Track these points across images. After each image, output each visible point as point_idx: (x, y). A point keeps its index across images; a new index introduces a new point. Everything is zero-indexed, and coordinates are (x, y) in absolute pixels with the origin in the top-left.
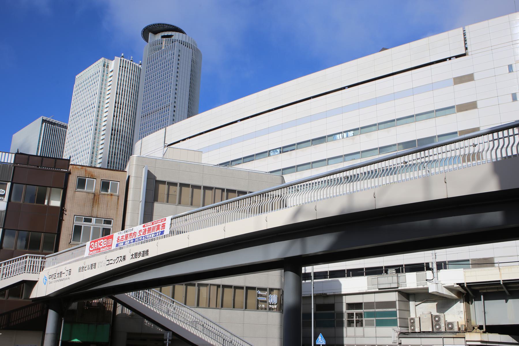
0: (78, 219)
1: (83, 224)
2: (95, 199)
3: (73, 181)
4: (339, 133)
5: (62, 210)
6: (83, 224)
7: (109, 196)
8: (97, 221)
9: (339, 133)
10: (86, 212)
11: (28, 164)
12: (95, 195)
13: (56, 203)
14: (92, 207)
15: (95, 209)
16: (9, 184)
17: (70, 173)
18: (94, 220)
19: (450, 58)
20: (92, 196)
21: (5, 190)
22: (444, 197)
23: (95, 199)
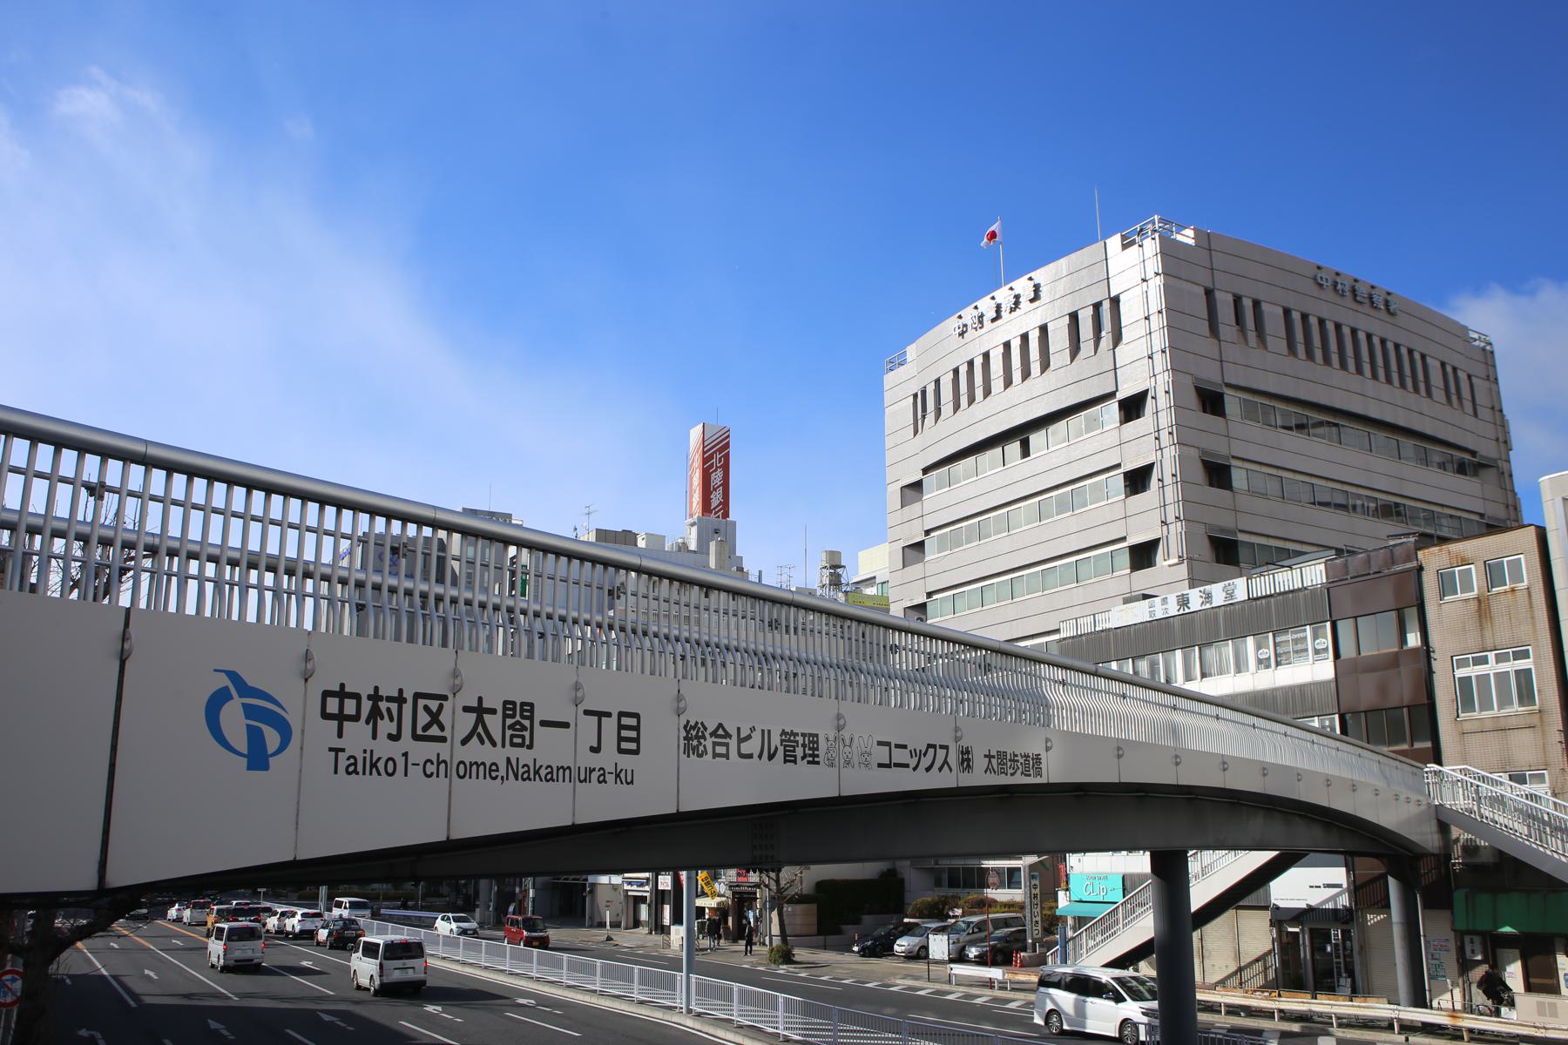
5: (1426, 649)
15: (1488, 634)
18: (1491, 656)
20: (1473, 606)
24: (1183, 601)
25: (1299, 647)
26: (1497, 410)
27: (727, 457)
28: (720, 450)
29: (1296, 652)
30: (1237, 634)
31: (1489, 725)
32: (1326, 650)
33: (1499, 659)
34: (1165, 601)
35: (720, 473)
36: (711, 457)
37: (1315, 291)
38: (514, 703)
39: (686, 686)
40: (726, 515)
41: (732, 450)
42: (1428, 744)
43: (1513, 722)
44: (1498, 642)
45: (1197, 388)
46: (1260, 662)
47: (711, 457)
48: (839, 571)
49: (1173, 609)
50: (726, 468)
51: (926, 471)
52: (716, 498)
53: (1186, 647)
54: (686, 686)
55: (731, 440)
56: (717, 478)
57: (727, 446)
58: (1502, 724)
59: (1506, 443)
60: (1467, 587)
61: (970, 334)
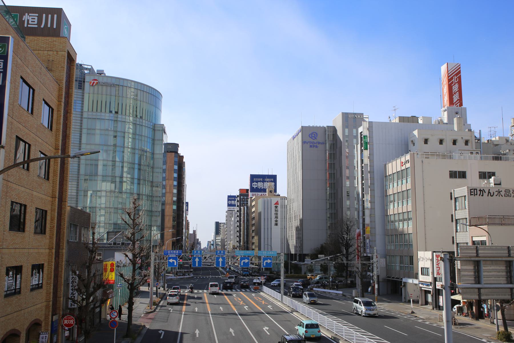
27: (460, 78)
28: (456, 75)
40: (461, 105)
41: (462, 74)
47: (452, 78)
52: (456, 98)
56: (455, 88)
57: (460, 72)
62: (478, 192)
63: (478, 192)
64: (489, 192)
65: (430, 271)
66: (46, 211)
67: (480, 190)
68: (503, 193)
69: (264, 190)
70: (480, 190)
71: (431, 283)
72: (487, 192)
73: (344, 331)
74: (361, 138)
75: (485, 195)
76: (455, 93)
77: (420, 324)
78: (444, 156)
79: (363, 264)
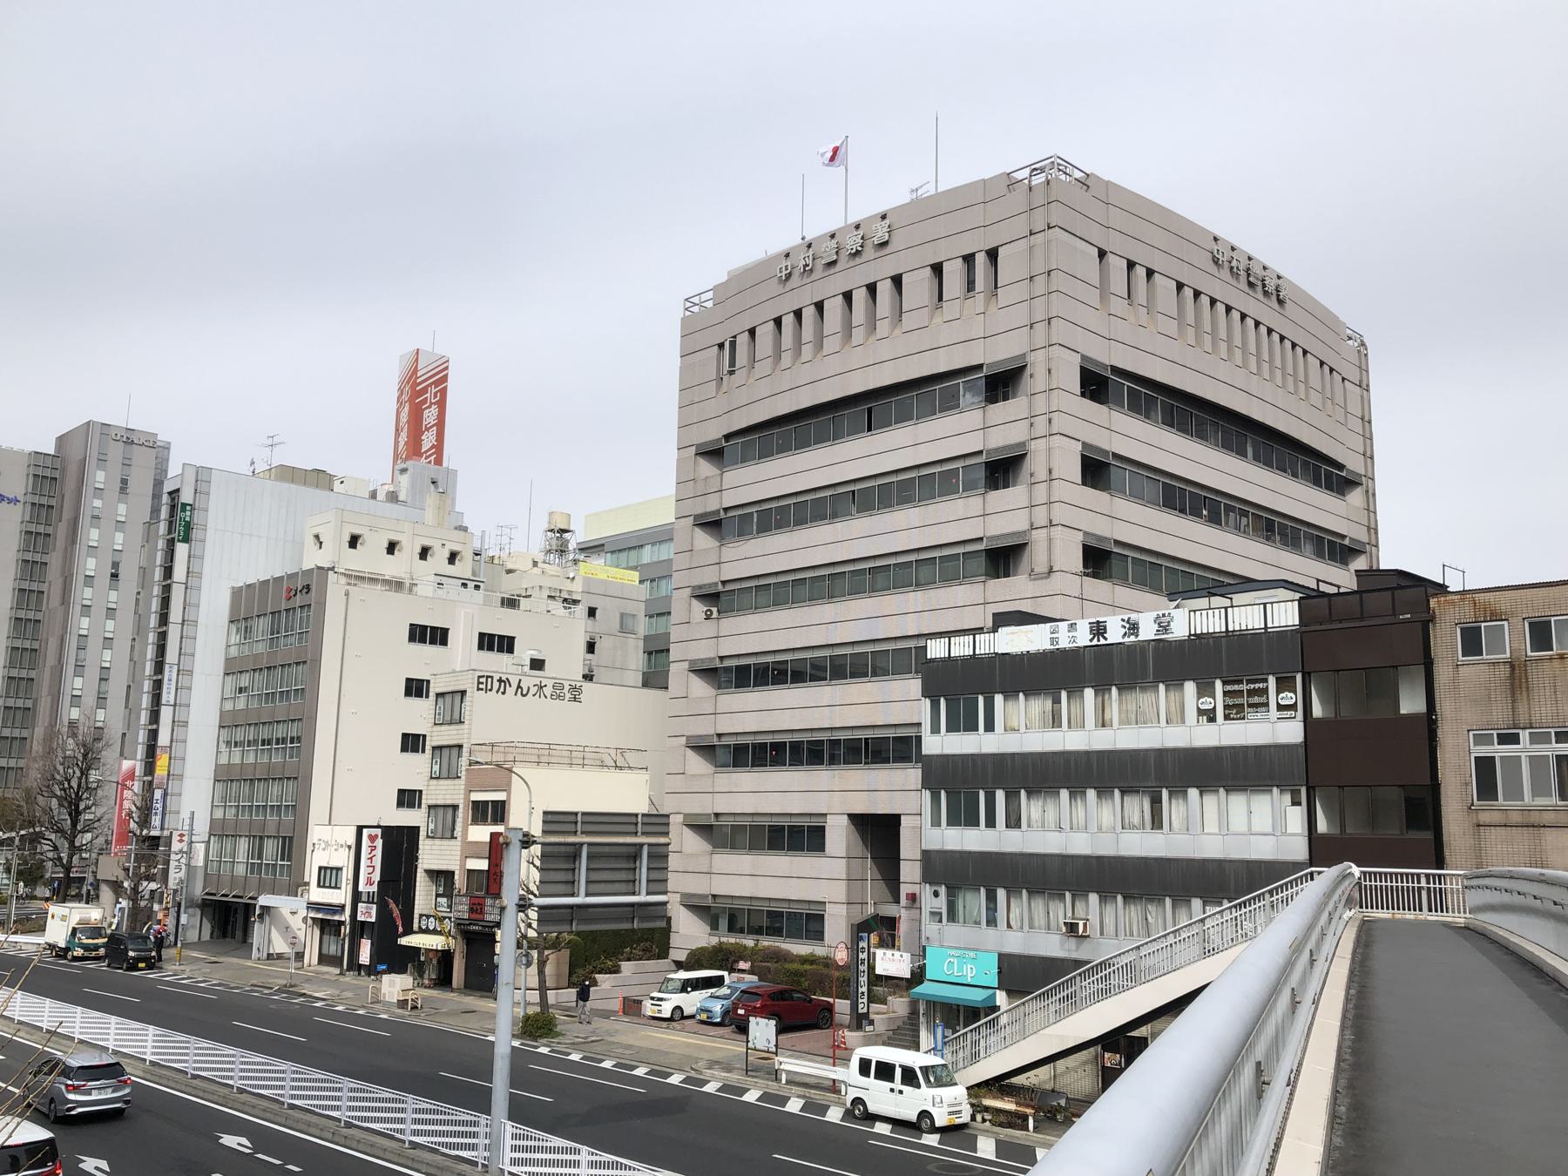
0: (1481, 740)
1: (1499, 751)
2: (1517, 676)
3: (1446, 640)
4: (940, 635)
5: (1429, 722)
6: (1499, 751)
7: (1556, 663)
8: (1534, 739)
9: (940, 635)
10: (1500, 715)
11: (1331, 621)
12: (1512, 667)
13: (1411, 703)
14: (1514, 701)
15: (1522, 708)
16: (1299, 677)
17: (1432, 619)
18: (1524, 735)
19: (373, 580)
20: (1504, 671)
21: (1295, 692)
22: (959, 848)
23: (1517, 676)
24: (1099, 629)
25: (1256, 700)
26: (1366, 421)
27: (444, 392)
28: (437, 383)
29: (1250, 706)
30: (1174, 680)
31: (1516, 818)
32: (1293, 707)
33: (1534, 739)
34: (1072, 627)
35: (434, 410)
36: (424, 390)
37: (1213, 269)
38: (870, 1061)
39: (20, 506)
40: (439, 462)
41: (451, 385)
42: (1429, 835)
43: (1548, 818)
44: (1535, 718)
45: (1083, 369)
46: (1201, 712)
47: (424, 390)
48: (566, 535)
49: (1083, 638)
50: (442, 405)
51: (728, 437)
52: (428, 440)
53: (1101, 688)
54: (20, 506)
55: (451, 373)
56: (430, 416)
57: (444, 379)
58: (1535, 818)
59: (1369, 457)
60: (1498, 646)
61: (795, 281)
62: (496, 685)
63: (496, 685)
64: (519, 687)
65: (347, 875)
66: (319, 885)
67: (500, 681)
68: (548, 691)
69: (1095, 384)
70: (500, 681)
71: (343, 907)
72: (514, 686)
73: (111, 1037)
74: (173, 507)
75: (511, 691)
76: (427, 429)
77: (319, 1010)
78: (397, 585)
79: (482, 912)
